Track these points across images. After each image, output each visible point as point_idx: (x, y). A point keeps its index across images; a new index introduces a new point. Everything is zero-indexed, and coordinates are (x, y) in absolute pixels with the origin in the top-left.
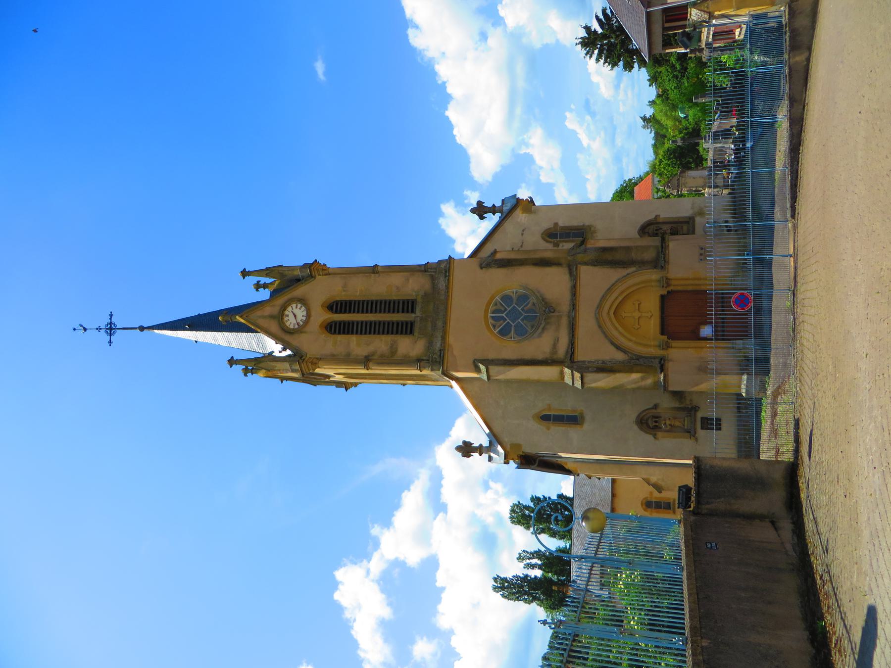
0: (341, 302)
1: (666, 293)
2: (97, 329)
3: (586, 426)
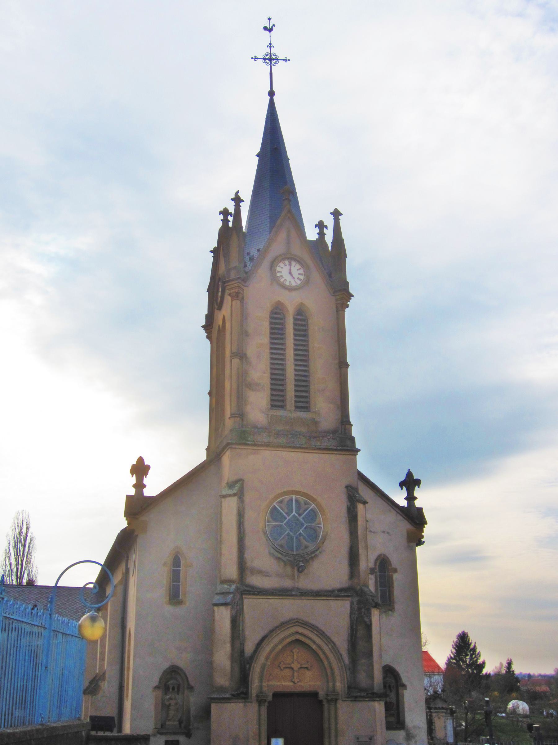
0: (307, 325)
1: (320, 699)
2: (270, 44)
3: (169, 609)
